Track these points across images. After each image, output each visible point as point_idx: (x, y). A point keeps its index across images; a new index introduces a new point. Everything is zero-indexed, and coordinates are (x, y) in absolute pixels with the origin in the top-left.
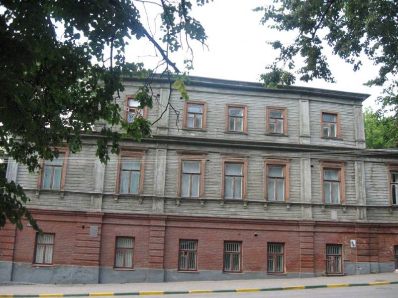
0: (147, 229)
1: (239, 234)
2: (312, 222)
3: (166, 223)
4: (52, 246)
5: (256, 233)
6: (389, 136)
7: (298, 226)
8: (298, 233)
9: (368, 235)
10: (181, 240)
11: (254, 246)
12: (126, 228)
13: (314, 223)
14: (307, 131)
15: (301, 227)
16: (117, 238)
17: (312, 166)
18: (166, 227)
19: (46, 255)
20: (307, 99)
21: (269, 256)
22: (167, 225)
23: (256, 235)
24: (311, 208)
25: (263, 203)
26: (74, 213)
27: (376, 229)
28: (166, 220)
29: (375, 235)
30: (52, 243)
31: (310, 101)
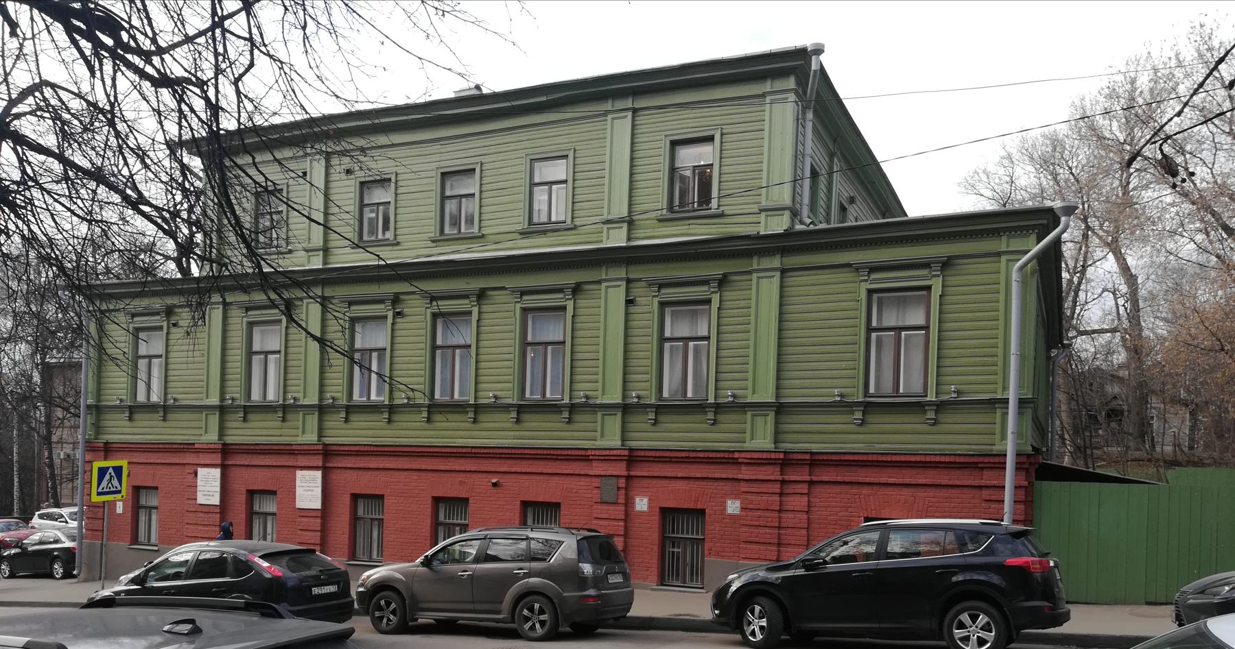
23: (495, 485)
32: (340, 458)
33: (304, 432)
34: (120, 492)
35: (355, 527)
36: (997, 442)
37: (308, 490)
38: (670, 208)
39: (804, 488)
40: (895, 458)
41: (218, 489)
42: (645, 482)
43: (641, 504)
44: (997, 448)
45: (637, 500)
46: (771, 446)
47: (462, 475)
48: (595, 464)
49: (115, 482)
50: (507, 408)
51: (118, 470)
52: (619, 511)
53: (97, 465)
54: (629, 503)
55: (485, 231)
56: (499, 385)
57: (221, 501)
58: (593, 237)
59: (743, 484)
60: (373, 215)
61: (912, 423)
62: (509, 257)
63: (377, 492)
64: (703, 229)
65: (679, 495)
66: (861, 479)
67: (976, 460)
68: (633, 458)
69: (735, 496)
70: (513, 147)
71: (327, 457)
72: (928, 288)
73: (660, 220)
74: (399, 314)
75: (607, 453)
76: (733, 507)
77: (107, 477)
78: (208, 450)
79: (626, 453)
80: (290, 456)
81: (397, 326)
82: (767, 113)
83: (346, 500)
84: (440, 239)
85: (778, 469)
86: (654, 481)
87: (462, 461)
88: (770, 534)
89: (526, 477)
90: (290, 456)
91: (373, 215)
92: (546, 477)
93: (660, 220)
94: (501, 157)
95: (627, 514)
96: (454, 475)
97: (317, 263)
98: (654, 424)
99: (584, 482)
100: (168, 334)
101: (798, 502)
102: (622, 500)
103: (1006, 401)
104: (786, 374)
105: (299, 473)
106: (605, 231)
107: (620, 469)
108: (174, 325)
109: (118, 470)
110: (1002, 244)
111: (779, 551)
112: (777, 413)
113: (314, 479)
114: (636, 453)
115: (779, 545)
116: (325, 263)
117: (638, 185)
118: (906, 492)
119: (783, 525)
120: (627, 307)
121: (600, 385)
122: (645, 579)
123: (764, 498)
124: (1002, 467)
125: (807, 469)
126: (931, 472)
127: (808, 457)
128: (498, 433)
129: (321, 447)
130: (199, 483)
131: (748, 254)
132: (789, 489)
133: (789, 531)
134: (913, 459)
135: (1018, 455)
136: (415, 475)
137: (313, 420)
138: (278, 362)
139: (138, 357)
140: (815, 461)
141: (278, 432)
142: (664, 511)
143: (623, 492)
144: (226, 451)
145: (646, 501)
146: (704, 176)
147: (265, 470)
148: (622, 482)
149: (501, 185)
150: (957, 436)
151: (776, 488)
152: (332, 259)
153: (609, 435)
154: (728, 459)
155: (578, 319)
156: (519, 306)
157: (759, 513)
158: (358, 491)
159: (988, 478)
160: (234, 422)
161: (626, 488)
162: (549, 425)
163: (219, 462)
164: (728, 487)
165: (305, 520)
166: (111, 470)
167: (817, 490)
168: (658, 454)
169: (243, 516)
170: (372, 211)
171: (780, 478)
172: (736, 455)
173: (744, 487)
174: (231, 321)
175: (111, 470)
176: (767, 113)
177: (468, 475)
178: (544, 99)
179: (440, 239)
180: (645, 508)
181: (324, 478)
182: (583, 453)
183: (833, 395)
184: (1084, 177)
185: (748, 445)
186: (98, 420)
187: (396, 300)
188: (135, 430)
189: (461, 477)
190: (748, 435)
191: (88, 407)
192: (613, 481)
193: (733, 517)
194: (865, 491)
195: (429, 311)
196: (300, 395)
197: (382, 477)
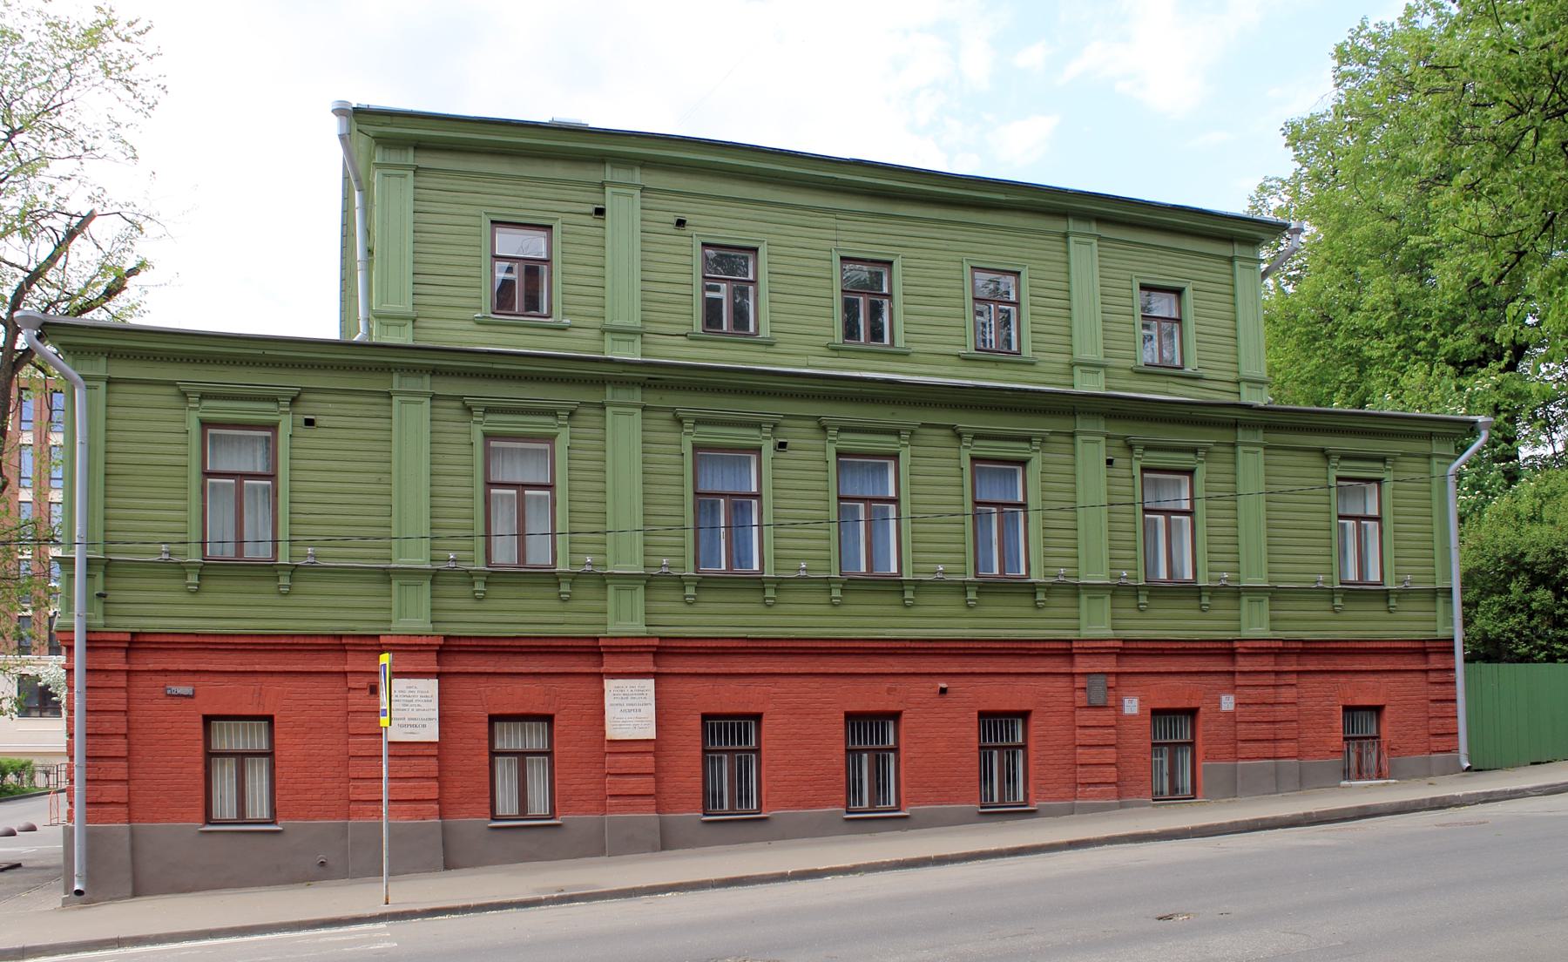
0: (1062, 683)
1: (889, 691)
2: (1111, 644)
3: (655, 664)
4: (265, 760)
5: (944, 685)
6: (1523, 378)
7: (594, 659)
8: (1068, 679)
9: (1271, 680)
10: (705, 717)
11: (937, 724)
12: (520, 686)
13: (1120, 644)
14: (629, 316)
15: (1240, 659)
16: (208, 720)
17: (1109, 462)
18: (128, 672)
19: (246, 793)
20: (635, 186)
21: (985, 752)
22: (134, 668)
23: (943, 691)
24: (1108, 599)
25: (963, 587)
26: (331, 641)
27: (1294, 658)
28: (439, 653)
29: (1293, 679)
30: (264, 746)
31: (417, 170)
32: (459, 657)
39: (121, 680)
41: (436, 715)
42: (1134, 680)
43: (1131, 706)
44: (1442, 633)
47: (892, 679)
48: (350, 656)
50: (182, 569)
54: (1119, 707)
56: (813, 552)
61: (1376, 610)
62: (977, 387)
63: (752, 709)
64: (1182, 390)
66: (470, 669)
70: (943, 244)
73: (1137, 372)
74: (783, 445)
76: (1228, 703)
80: (596, 656)
85: (434, 656)
87: (890, 660)
90: (596, 656)
93: (1137, 372)
94: (927, 254)
96: (879, 680)
103: (1449, 591)
105: (609, 684)
112: (433, 583)
113: (642, 693)
122: (1139, 794)
123: (1260, 690)
124: (1450, 651)
125: (651, 658)
126: (1391, 659)
131: (600, 382)
134: (1381, 645)
136: (814, 683)
142: (1156, 712)
145: (1136, 701)
146: (532, 270)
149: (931, 291)
150: (1408, 624)
154: (1227, 650)
157: (1255, 708)
159: (1435, 662)
162: (1017, 610)
164: (1221, 681)
171: (126, 667)
173: (1240, 680)
178: (1002, 197)
180: (1135, 711)
183: (161, 552)
185: (1245, 634)
189: (887, 684)
193: (1230, 715)
194: (1342, 679)
197: (276, 687)
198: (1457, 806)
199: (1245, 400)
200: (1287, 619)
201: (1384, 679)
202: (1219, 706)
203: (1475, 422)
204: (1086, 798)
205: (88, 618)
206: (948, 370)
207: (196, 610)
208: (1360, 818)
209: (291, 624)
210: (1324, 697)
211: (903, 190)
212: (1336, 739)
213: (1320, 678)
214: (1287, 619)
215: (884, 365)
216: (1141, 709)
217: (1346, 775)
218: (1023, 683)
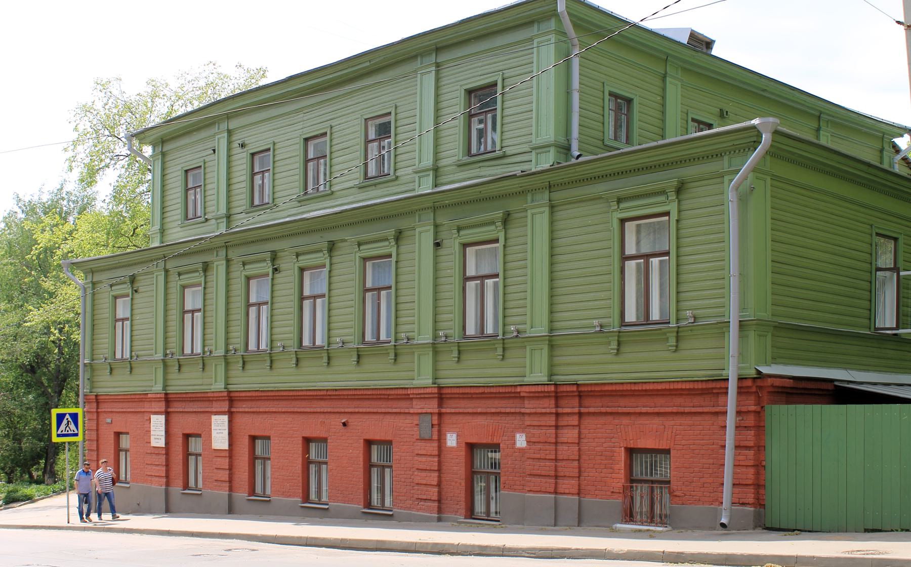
23: (344, 424)
33: (216, 381)
34: (76, 435)
35: (119, 455)
36: (527, 375)
37: (219, 432)
38: (469, 153)
40: (645, 387)
42: (454, 419)
43: (451, 440)
45: (448, 435)
46: (544, 379)
47: (322, 416)
49: (72, 426)
51: (74, 417)
52: (433, 448)
53: (55, 412)
54: (441, 440)
55: (334, 189)
57: (166, 444)
58: (410, 186)
59: (527, 418)
60: (482, 126)
65: (480, 429)
67: (711, 385)
68: (442, 395)
69: (522, 429)
71: (231, 402)
72: (667, 214)
73: (459, 166)
75: (422, 391)
76: (521, 441)
77: (65, 422)
78: (218, 399)
79: (436, 391)
81: (276, 281)
82: (535, 55)
83: (246, 441)
84: (305, 198)
86: (461, 417)
88: (547, 467)
89: (366, 417)
91: (482, 126)
92: (381, 416)
93: (459, 166)
95: (440, 448)
97: (426, 187)
98: (617, 354)
99: (409, 420)
100: (273, 279)
101: (570, 435)
102: (435, 437)
104: (558, 308)
105: (214, 418)
106: (417, 179)
107: (548, 405)
108: (136, 291)
109: (74, 417)
110: (724, 164)
111: (556, 484)
114: (445, 391)
115: (556, 477)
116: (228, 227)
117: (443, 134)
118: (657, 421)
119: (560, 457)
120: (435, 251)
121: (416, 326)
122: (456, 512)
127: (575, 388)
128: (345, 376)
129: (552, 388)
130: (152, 428)
132: (563, 421)
133: (564, 463)
134: (660, 387)
135: (741, 379)
137: (427, 361)
138: (388, 296)
139: (302, 298)
140: (582, 393)
141: (199, 382)
143: (436, 429)
144: (168, 399)
145: (455, 436)
147: (194, 415)
148: (435, 418)
150: (691, 364)
151: (551, 421)
152: (166, 239)
153: (421, 376)
154: (510, 393)
155: (684, 223)
156: (358, 255)
158: (257, 434)
160: (448, 360)
161: (439, 425)
163: (163, 410)
165: (219, 459)
166: (67, 416)
167: (587, 422)
168: (461, 391)
169: (181, 457)
170: (481, 122)
172: (519, 389)
173: (528, 421)
174: (233, 275)
175: (67, 416)
176: (535, 55)
177: (327, 416)
179: (305, 198)
181: (230, 421)
182: (404, 392)
184: (56, 260)
186: (92, 376)
187: (133, 280)
188: (329, 377)
190: (528, 370)
191: (85, 365)
192: (428, 418)
193: (521, 450)
194: (625, 421)
195: (296, 265)
196: (213, 348)
198: (452, 554)
199: (823, 141)
200: (568, 364)
201: (670, 422)
202: (515, 443)
203: (754, 127)
204: (418, 510)
205: (739, 368)
206: (350, 199)
207: (329, 377)
208: (440, 553)
209: (131, 389)
210: (607, 439)
211: (317, 84)
212: (619, 479)
213: (602, 420)
214: (568, 364)
215: (321, 205)
216: (458, 442)
217: (629, 516)
218: (388, 419)
